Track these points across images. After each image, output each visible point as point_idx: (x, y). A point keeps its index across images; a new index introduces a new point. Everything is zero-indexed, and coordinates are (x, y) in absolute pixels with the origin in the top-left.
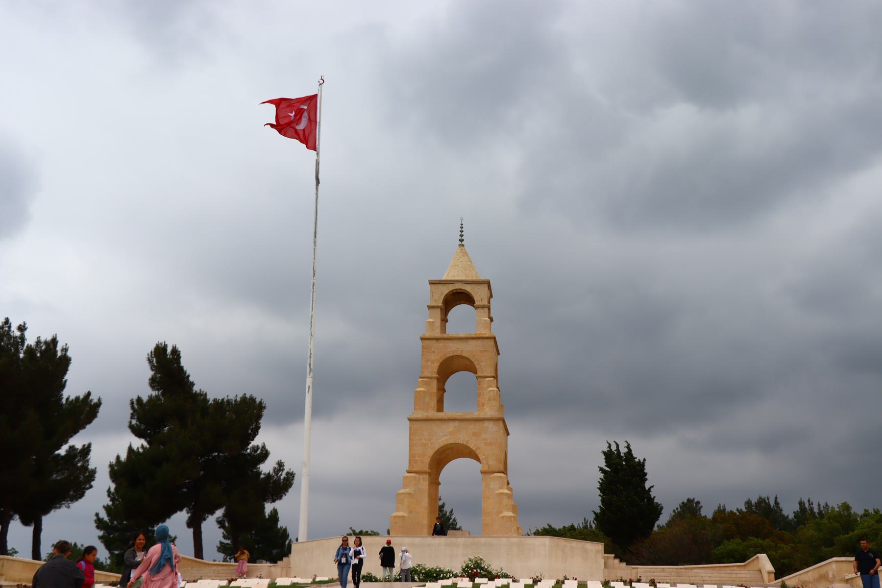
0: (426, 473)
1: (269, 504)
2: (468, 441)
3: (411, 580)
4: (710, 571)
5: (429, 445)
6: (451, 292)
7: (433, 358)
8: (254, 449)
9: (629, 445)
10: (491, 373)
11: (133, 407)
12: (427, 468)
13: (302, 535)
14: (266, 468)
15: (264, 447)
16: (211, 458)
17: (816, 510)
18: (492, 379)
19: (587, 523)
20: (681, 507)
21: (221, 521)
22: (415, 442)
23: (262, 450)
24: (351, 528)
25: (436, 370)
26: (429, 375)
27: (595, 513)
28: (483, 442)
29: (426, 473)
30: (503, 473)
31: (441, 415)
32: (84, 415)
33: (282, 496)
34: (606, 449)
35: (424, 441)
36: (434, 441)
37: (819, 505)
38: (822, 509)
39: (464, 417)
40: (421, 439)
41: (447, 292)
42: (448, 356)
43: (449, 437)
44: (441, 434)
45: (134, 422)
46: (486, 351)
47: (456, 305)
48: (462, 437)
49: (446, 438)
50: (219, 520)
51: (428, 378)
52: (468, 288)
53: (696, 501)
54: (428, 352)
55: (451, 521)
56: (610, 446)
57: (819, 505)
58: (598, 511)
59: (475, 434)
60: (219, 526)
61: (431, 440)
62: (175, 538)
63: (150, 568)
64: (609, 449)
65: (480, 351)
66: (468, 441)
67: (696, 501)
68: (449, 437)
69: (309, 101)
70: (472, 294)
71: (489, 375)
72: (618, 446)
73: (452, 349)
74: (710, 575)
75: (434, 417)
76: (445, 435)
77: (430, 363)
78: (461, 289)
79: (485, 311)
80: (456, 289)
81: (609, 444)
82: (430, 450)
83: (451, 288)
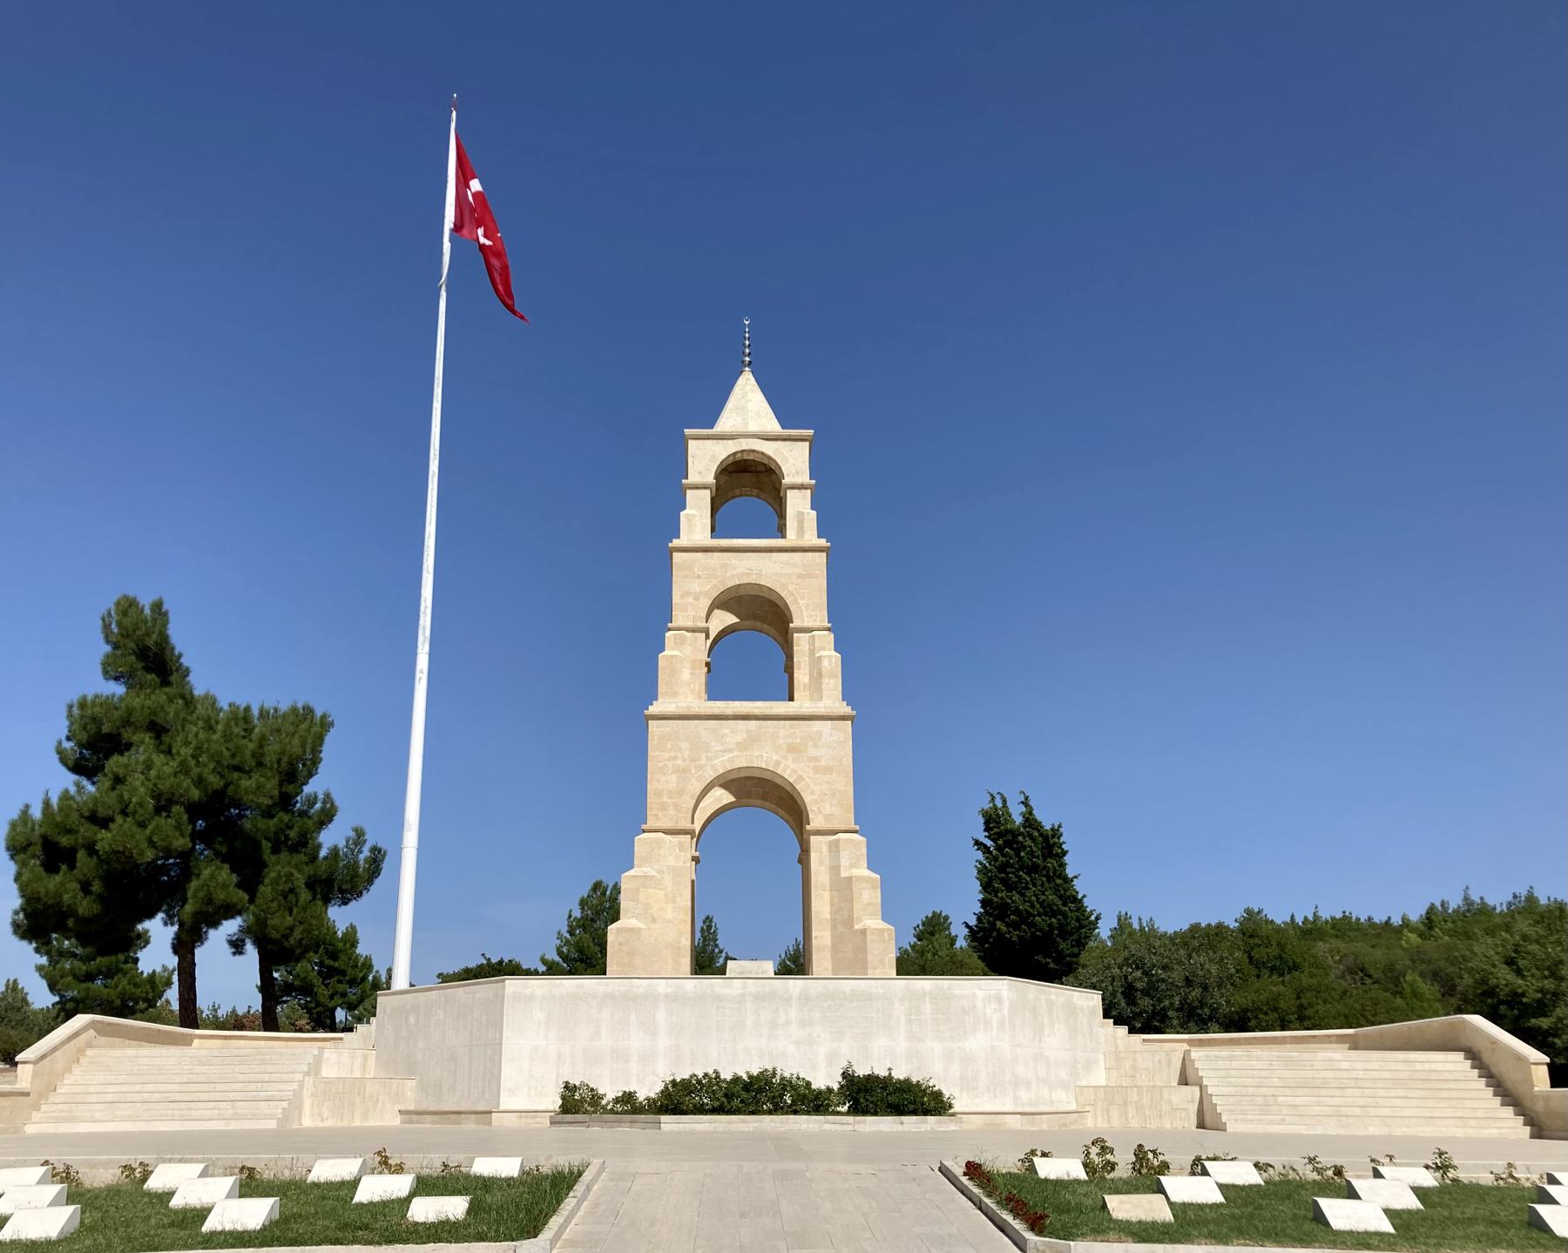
0: (843, 718)
1: (336, 907)
2: (778, 763)
5: (693, 771)
6: (731, 459)
7: (698, 590)
8: (309, 800)
9: (1027, 798)
10: (822, 621)
11: (70, 715)
13: (400, 981)
14: (331, 838)
15: (328, 796)
16: (222, 818)
17: (1136, 926)
18: (827, 632)
19: (799, 945)
20: (923, 924)
21: (237, 940)
22: (661, 764)
23: (324, 802)
24: (483, 955)
26: (689, 624)
27: (967, 926)
28: (812, 765)
29: (843, 718)
32: (998, 1212)
33: (361, 893)
34: (987, 806)
35: (680, 762)
36: (703, 762)
37: (1140, 919)
38: (1145, 924)
40: (675, 758)
41: (723, 457)
42: (730, 584)
43: (736, 753)
44: (718, 749)
45: (68, 745)
46: (810, 576)
48: (765, 755)
49: (728, 756)
50: (234, 939)
52: (769, 448)
53: (943, 914)
54: (686, 576)
55: (1147, 929)
56: (993, 798)
57: (1140, 919)
58: (973, 922)
59: (792, 749)
60: (233, 950)
61: (695, 761)
64: (991, 805)
65: (799, 576)
66: (778, 763)
67: (943, 914)
68: (736, 753)
71: (818, 624)
72: (1004, 801)
73: (738, 571)
76: (729, 750)
77: (690, 600)
78: (754, 451)
79: (804, 496)
80: (743, 451)
81: (991, 795)
82: (693, 780)
83: (730, 448)
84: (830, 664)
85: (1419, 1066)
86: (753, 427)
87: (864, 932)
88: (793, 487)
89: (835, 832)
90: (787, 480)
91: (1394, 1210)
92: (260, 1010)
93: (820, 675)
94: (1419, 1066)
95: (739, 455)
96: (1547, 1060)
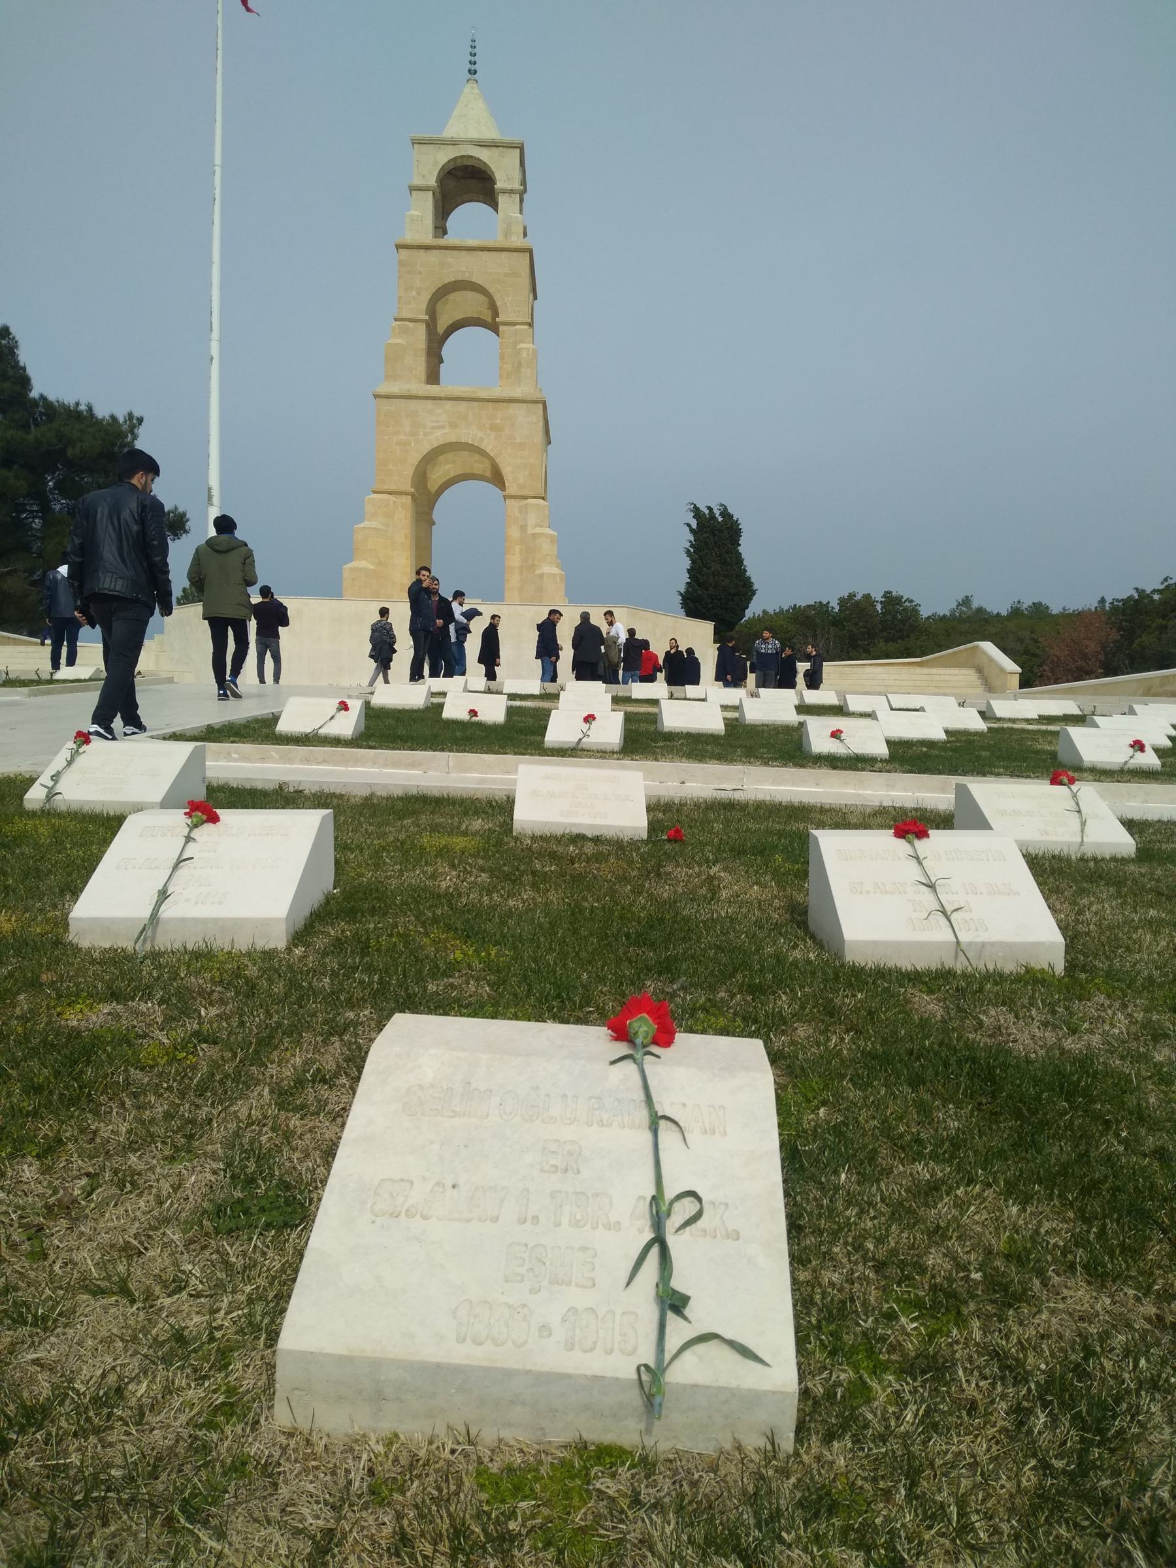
0: (406, 494)
2: (482, 440)
3: (539, 738)
4: (905, 669)
12: (409, 485)
25: (424, 307)
26: (411, 316)
29: (406, 494)
30: (543, 499)
31: (433, 389)
35: (402, 437)
39: (474, 396)
41: (446, 160)
47: (463, 203)
49: (439, 433)
51: (410, 320)
52: (484, 155)
62: (237, 696)
63: (517, 703)
66: (482, 440)
68: (447, 430)
69: (320, 731)
70: (492, 167)
74: (896, 677)
75: (421, 394)
84: (528, 355)
85: (937, 677)
86: (473, 134)
87: (541, 576)
88: (504, 192)
89: (526, 498)
90: (499, 185)
91: (625, 739)
92: (103, 668)
93: (520, 365)
94: (937, 677)
95: (459, 161)
96: (1019, 670)
